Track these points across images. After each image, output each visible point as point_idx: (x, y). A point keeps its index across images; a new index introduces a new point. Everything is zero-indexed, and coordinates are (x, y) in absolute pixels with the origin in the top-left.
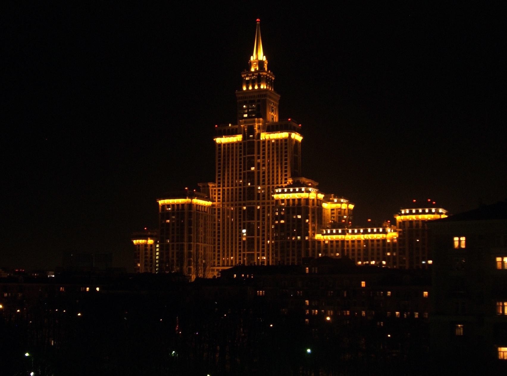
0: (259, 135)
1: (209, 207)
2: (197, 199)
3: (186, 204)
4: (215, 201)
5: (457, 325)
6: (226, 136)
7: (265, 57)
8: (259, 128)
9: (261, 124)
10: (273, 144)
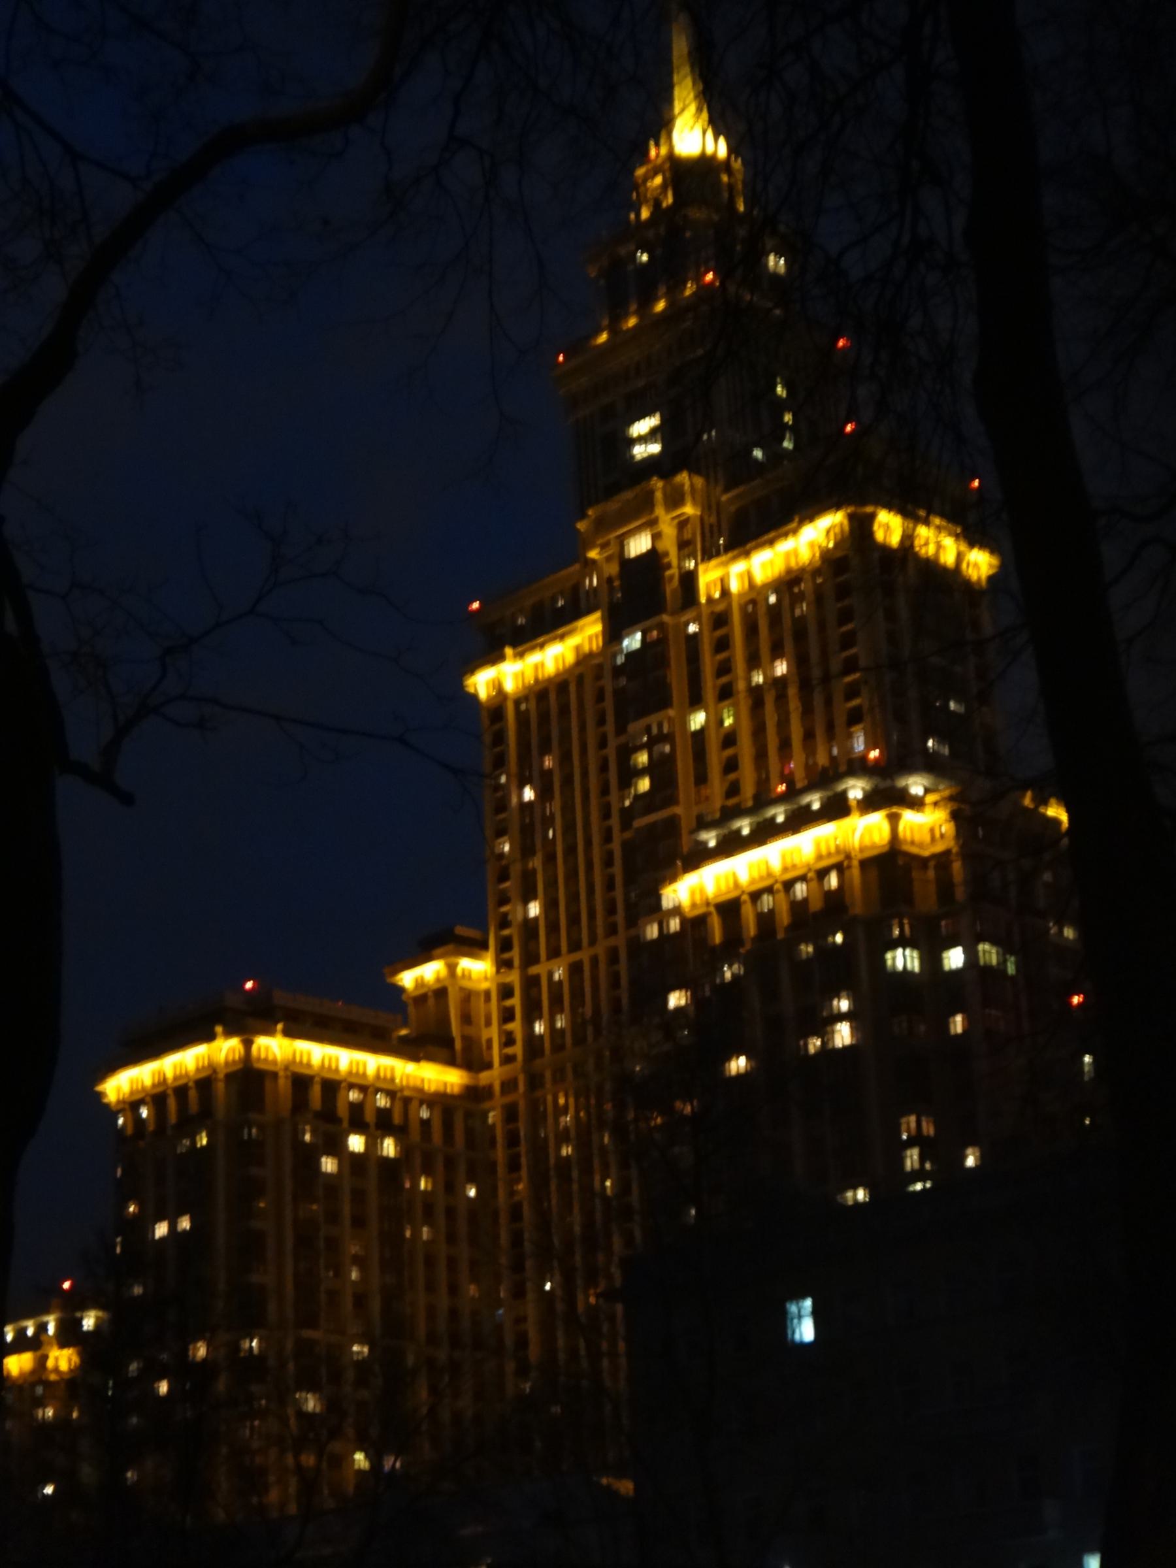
0: (689, 580)
1: (440, 1100)
2: (289, 1033)
3: (221, 1076)
4: (489, 1066)
5: (76, 1408)
6: (520, 649)
7: (722, 141)
8: (684, 545)
9: (689, 510)
10: (775, 613)
